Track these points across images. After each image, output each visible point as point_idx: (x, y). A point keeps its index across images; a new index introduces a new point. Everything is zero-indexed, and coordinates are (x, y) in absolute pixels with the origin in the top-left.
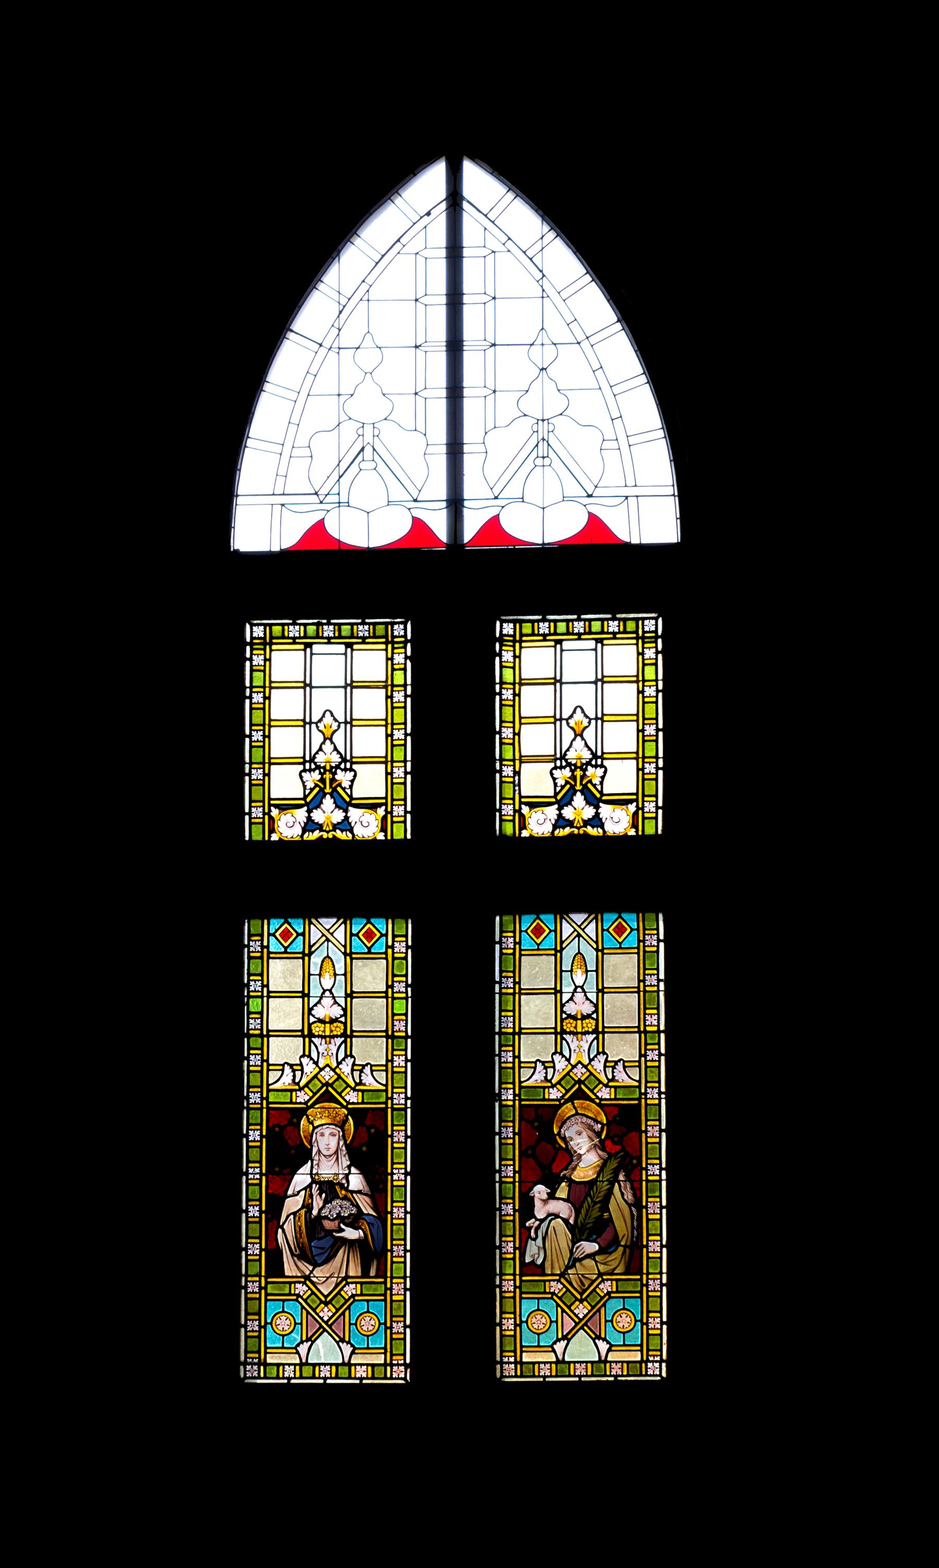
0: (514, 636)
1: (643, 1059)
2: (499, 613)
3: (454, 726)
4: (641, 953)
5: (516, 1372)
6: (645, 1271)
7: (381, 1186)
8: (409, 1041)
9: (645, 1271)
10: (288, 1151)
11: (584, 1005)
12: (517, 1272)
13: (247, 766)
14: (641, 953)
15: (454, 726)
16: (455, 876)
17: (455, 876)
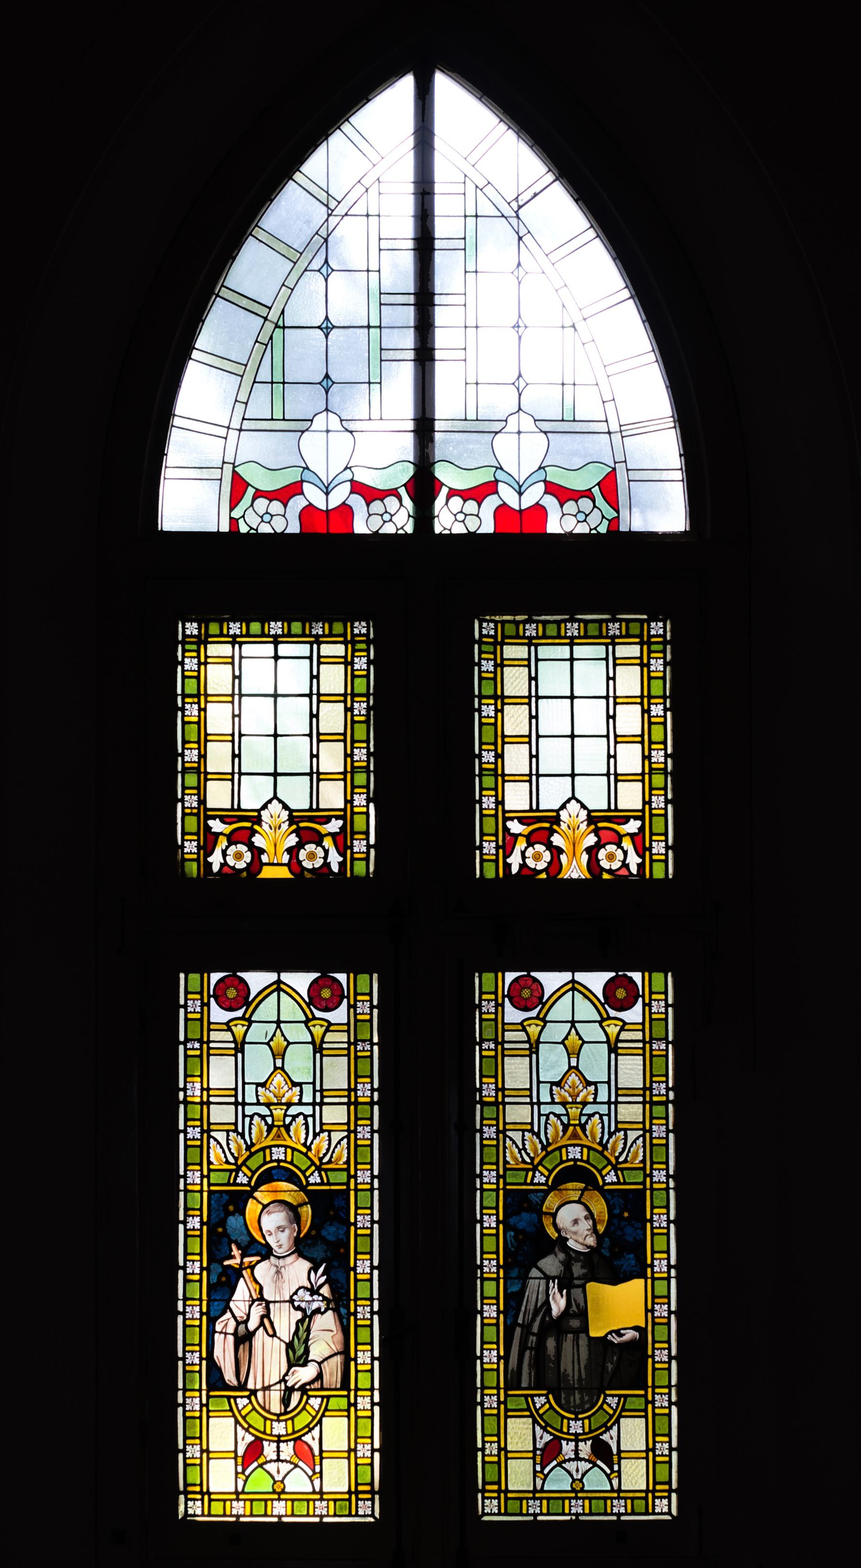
0: (495, 637)
1: (647, 807)
2: (481, 613)
3: (424, 743)
4: (648, 1055)
5: (499, 1509)
6: (650, 1384)
7: (342, 1251)
8: (376, 1108)
9: (650, 1384)
10: (230, 1243)
11: (579, 1058)
12: (502, 1385)
13: (179, 699)
14: (648, 1055)
15: (424, 743)
16: (424, 911)
17: (424, 911)
